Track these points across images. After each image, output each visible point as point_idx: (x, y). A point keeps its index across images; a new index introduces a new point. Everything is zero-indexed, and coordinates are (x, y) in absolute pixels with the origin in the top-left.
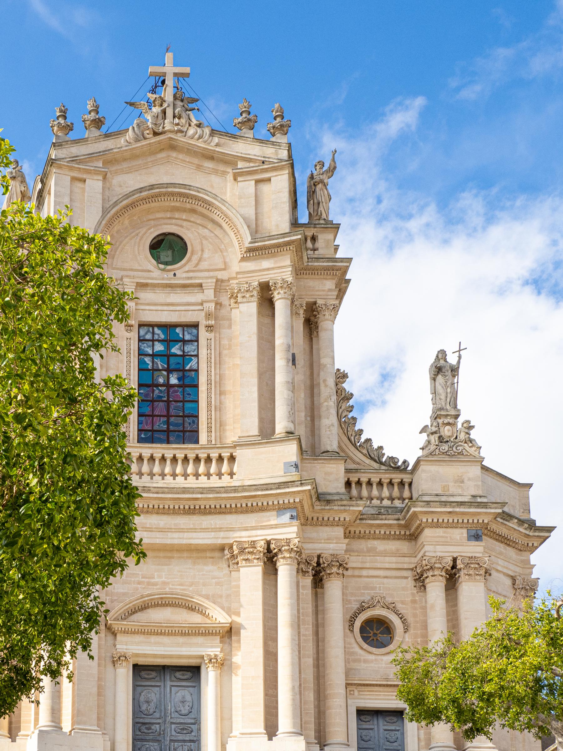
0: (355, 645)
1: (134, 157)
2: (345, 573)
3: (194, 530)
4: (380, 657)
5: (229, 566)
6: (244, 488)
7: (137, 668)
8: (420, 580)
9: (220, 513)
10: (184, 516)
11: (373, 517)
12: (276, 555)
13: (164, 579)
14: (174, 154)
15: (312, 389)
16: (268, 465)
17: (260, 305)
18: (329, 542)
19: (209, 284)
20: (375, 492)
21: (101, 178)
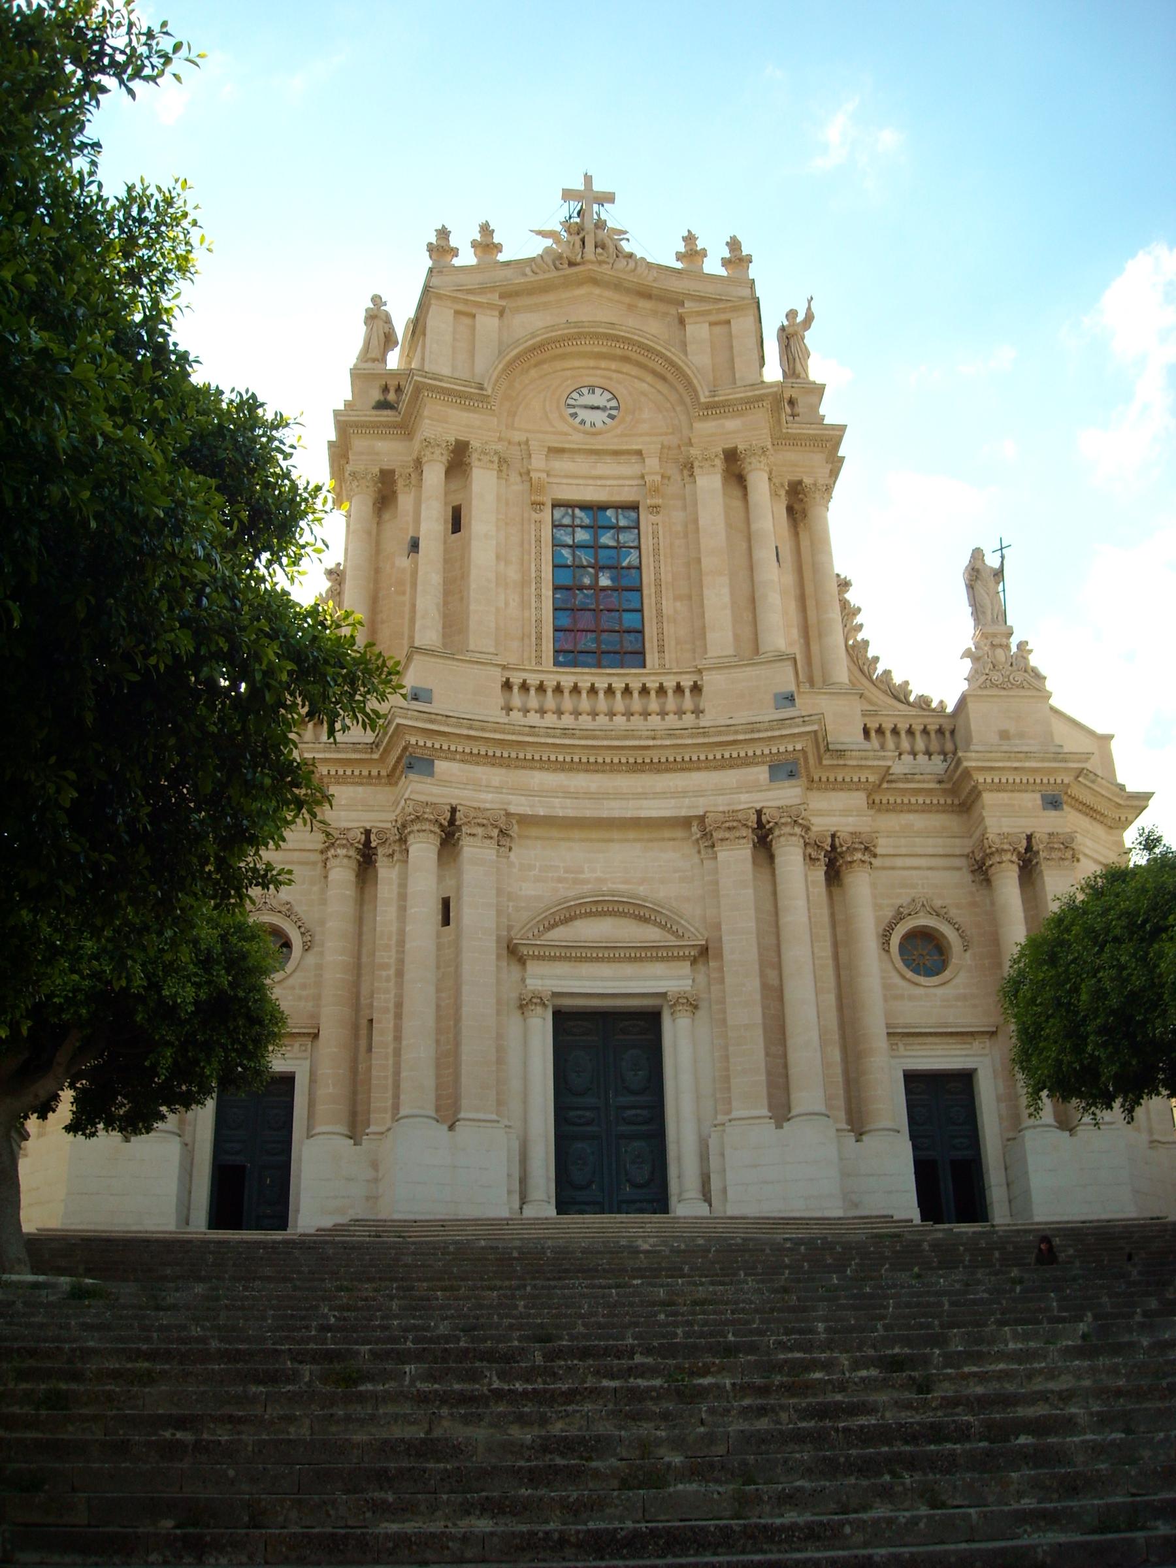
0: (894, 974)
2: (873, 860)
3: (643, 796)
4: (932, 990)
5: (699, 852)
9: (682, 769)
10: (628, 775)
12: (771, 830)
13: (599, 874)
14: (597, 291)
17: (726, 480)
21: (497, 313)
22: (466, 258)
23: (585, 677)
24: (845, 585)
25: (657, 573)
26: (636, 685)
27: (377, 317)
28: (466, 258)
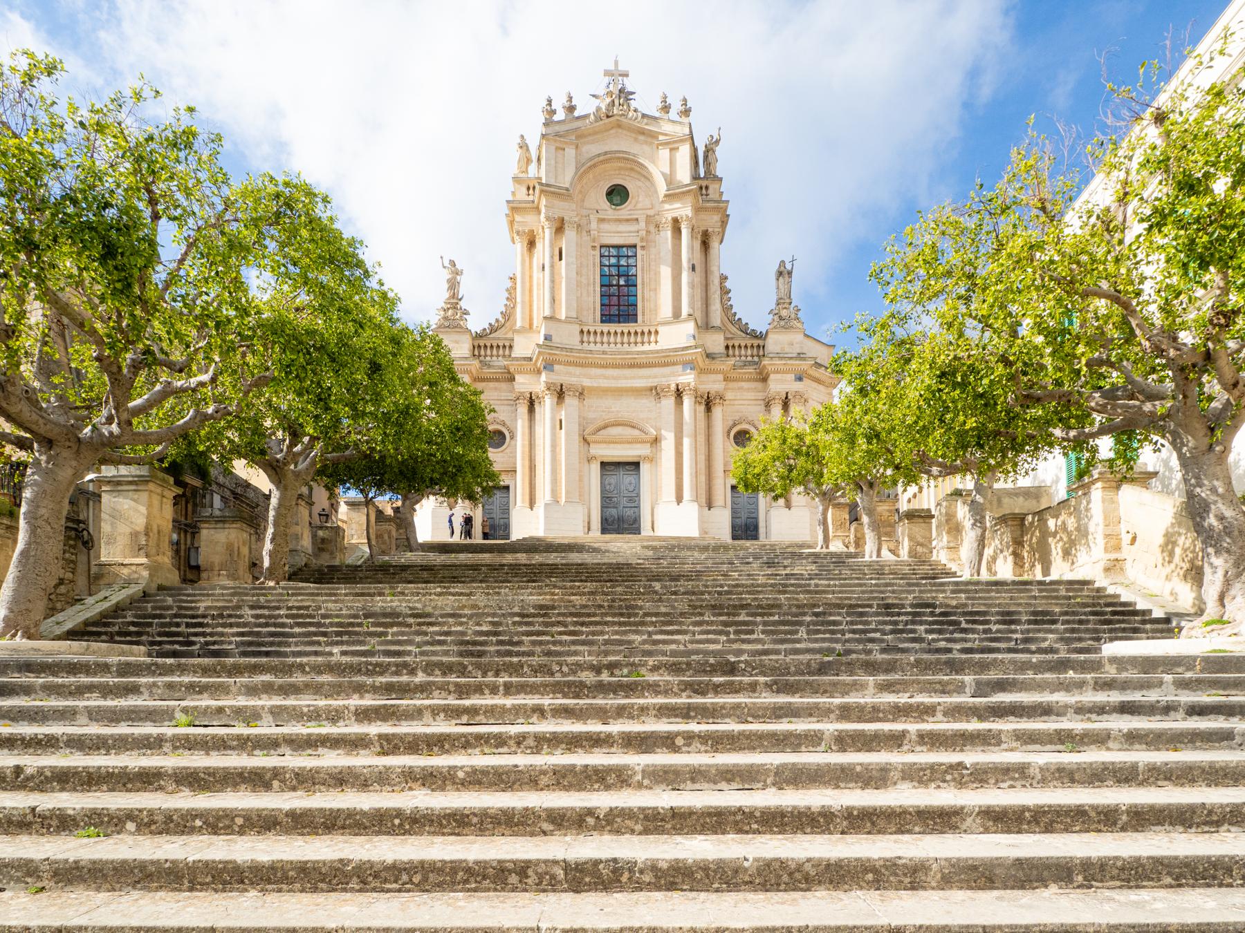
1: (595, 133)
3: (634, 378)
6: (662, 351)
7: (604, 465)
8: (768, 405)
11: (741, 367)
15: (706, 286)
16: (677, 335)
18: (714, 384)
19: (642, 219)
20: (743, 352)
22: (560, 115)
23: (613, 327)
26: (632, 331)
27: (524, 146)
28: (560, 115)
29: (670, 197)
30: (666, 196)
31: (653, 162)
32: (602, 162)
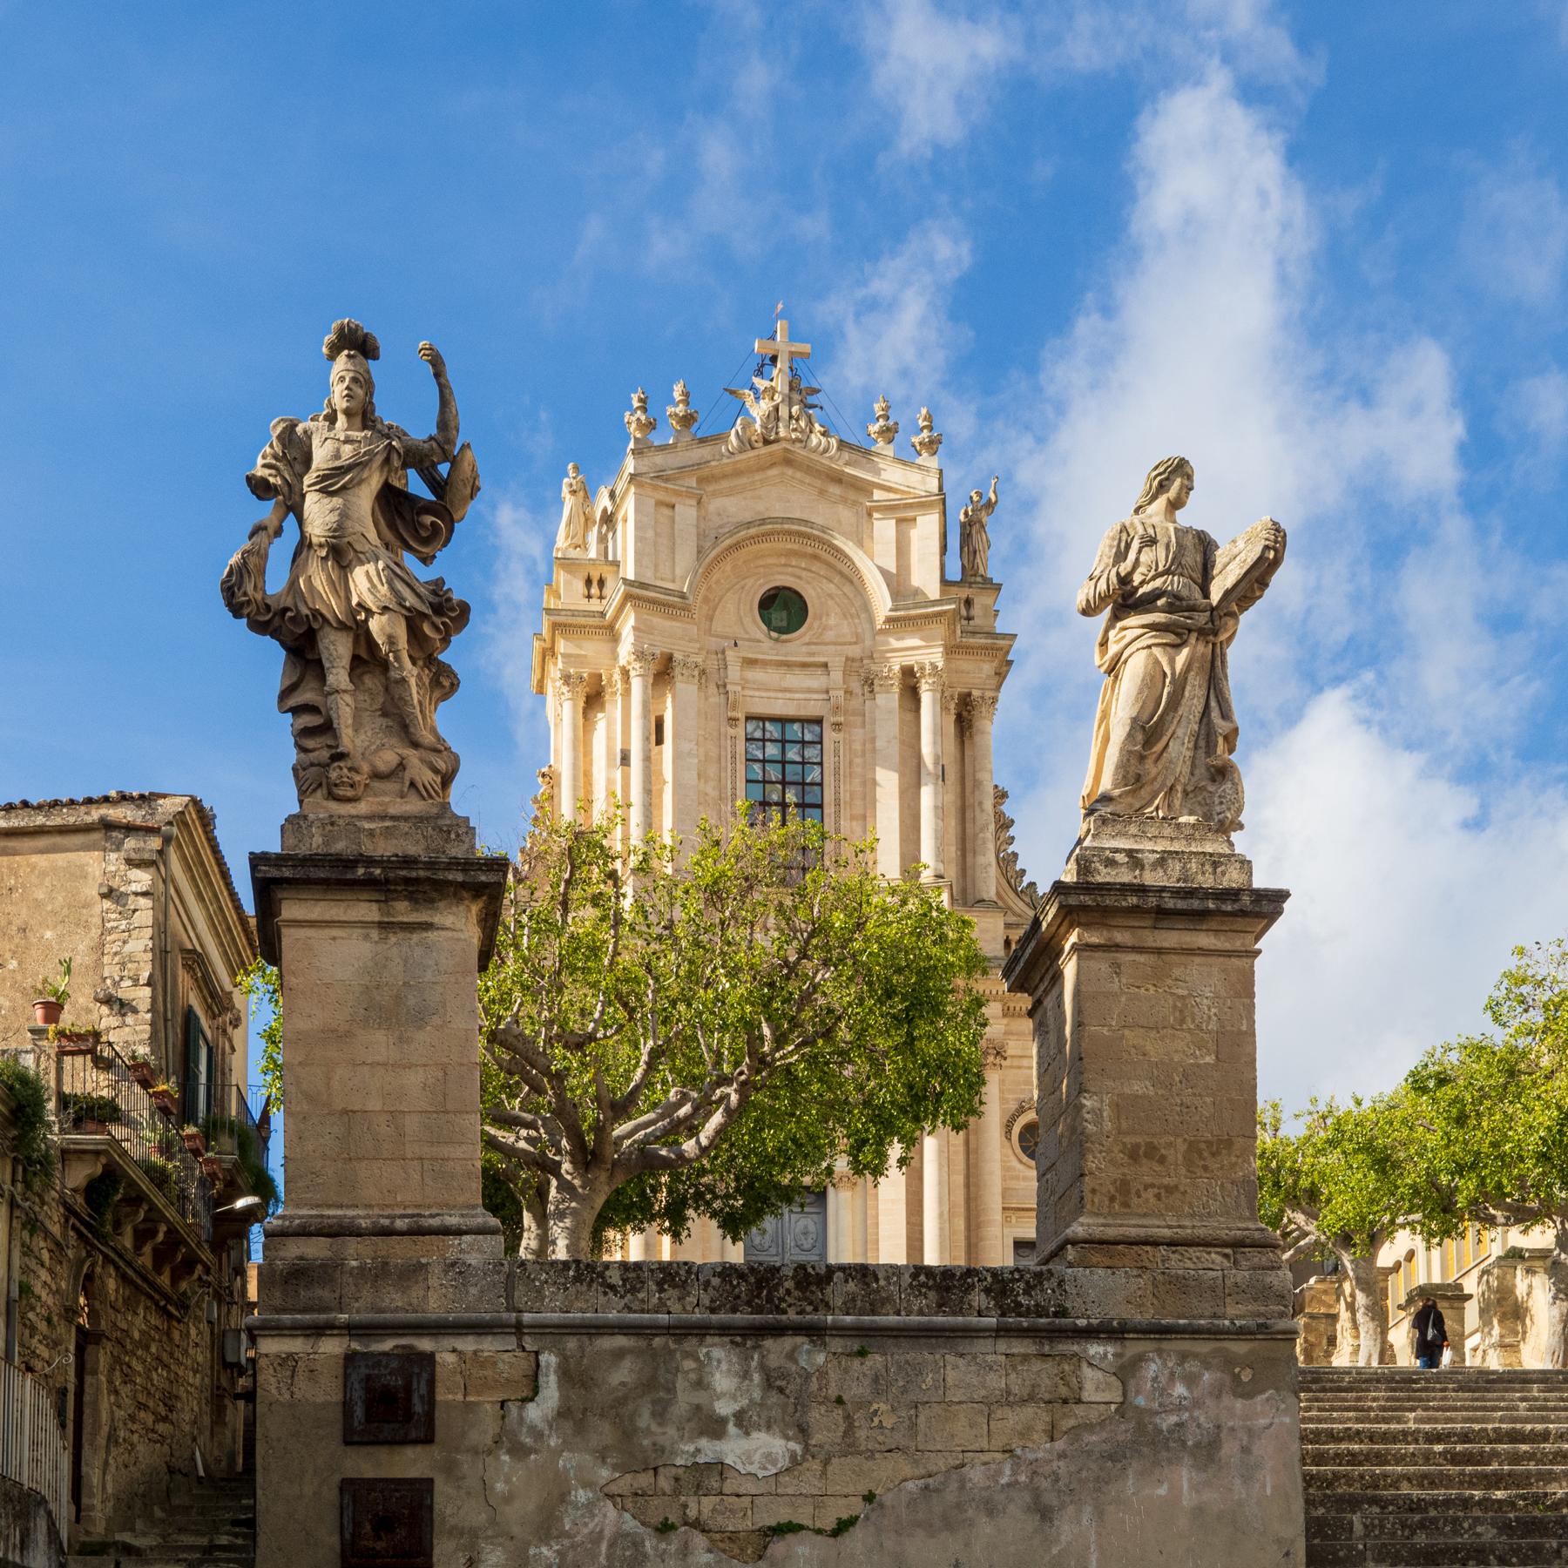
0: (1013, 1158)
1: (737, 473)
24: (1001, 795)
25: (837, 793)
29: (897, 623)
30: (889, 620)
31: (860, 544)
32: (753, 539)
